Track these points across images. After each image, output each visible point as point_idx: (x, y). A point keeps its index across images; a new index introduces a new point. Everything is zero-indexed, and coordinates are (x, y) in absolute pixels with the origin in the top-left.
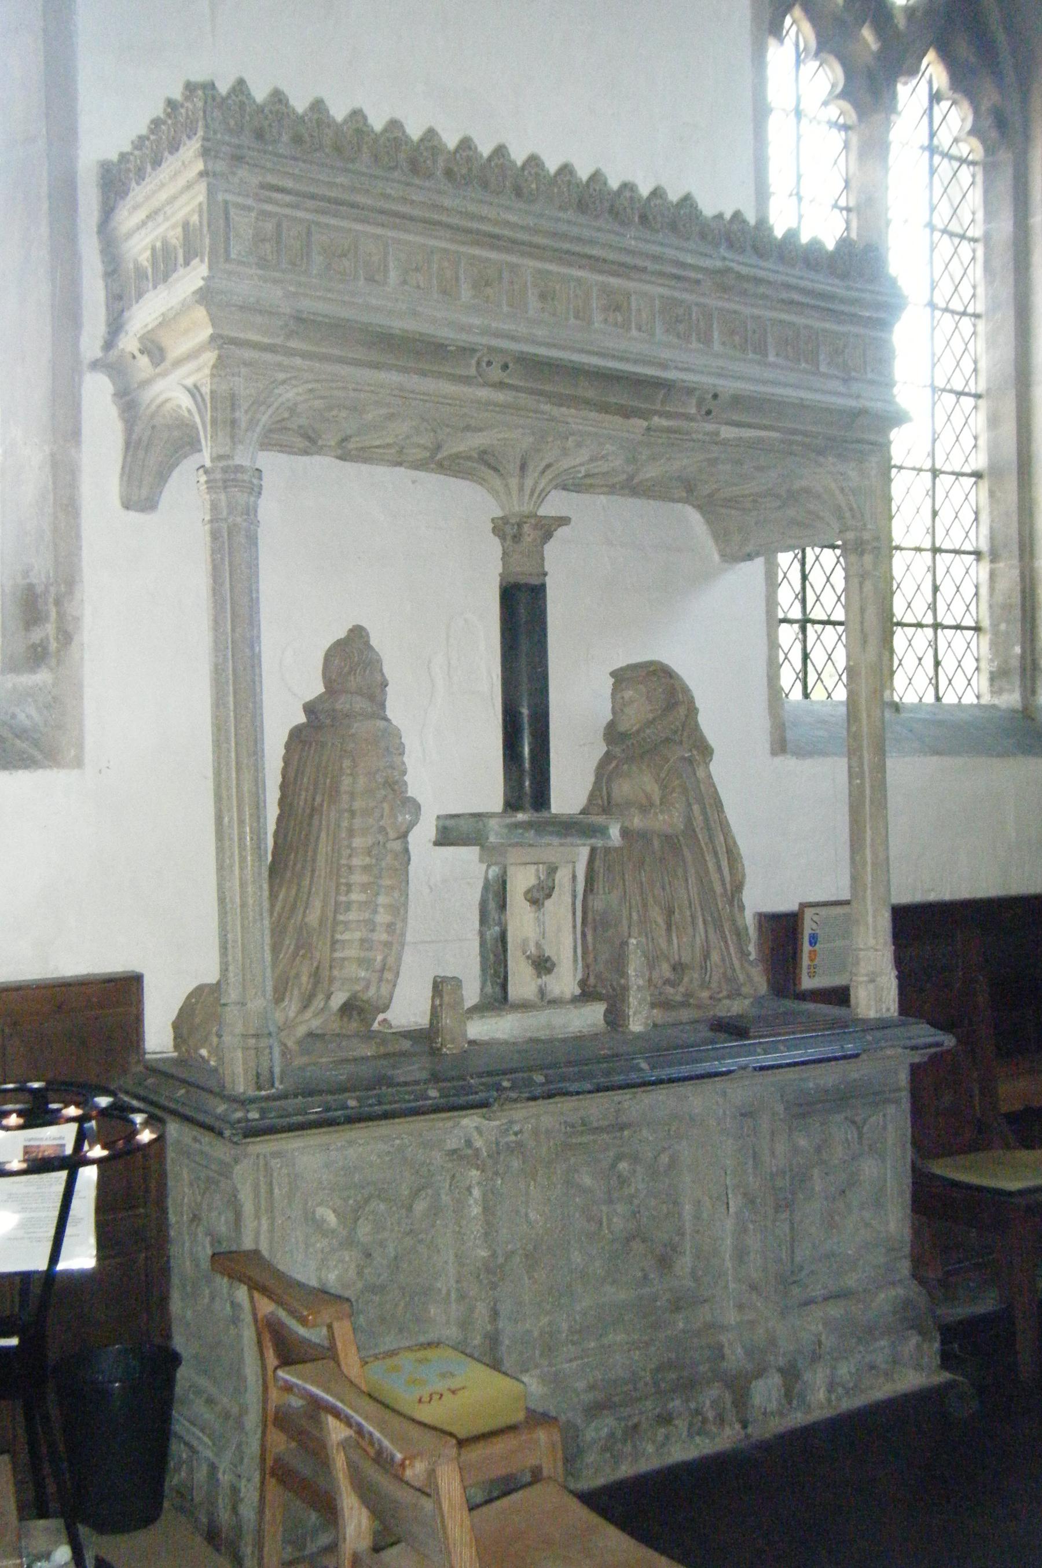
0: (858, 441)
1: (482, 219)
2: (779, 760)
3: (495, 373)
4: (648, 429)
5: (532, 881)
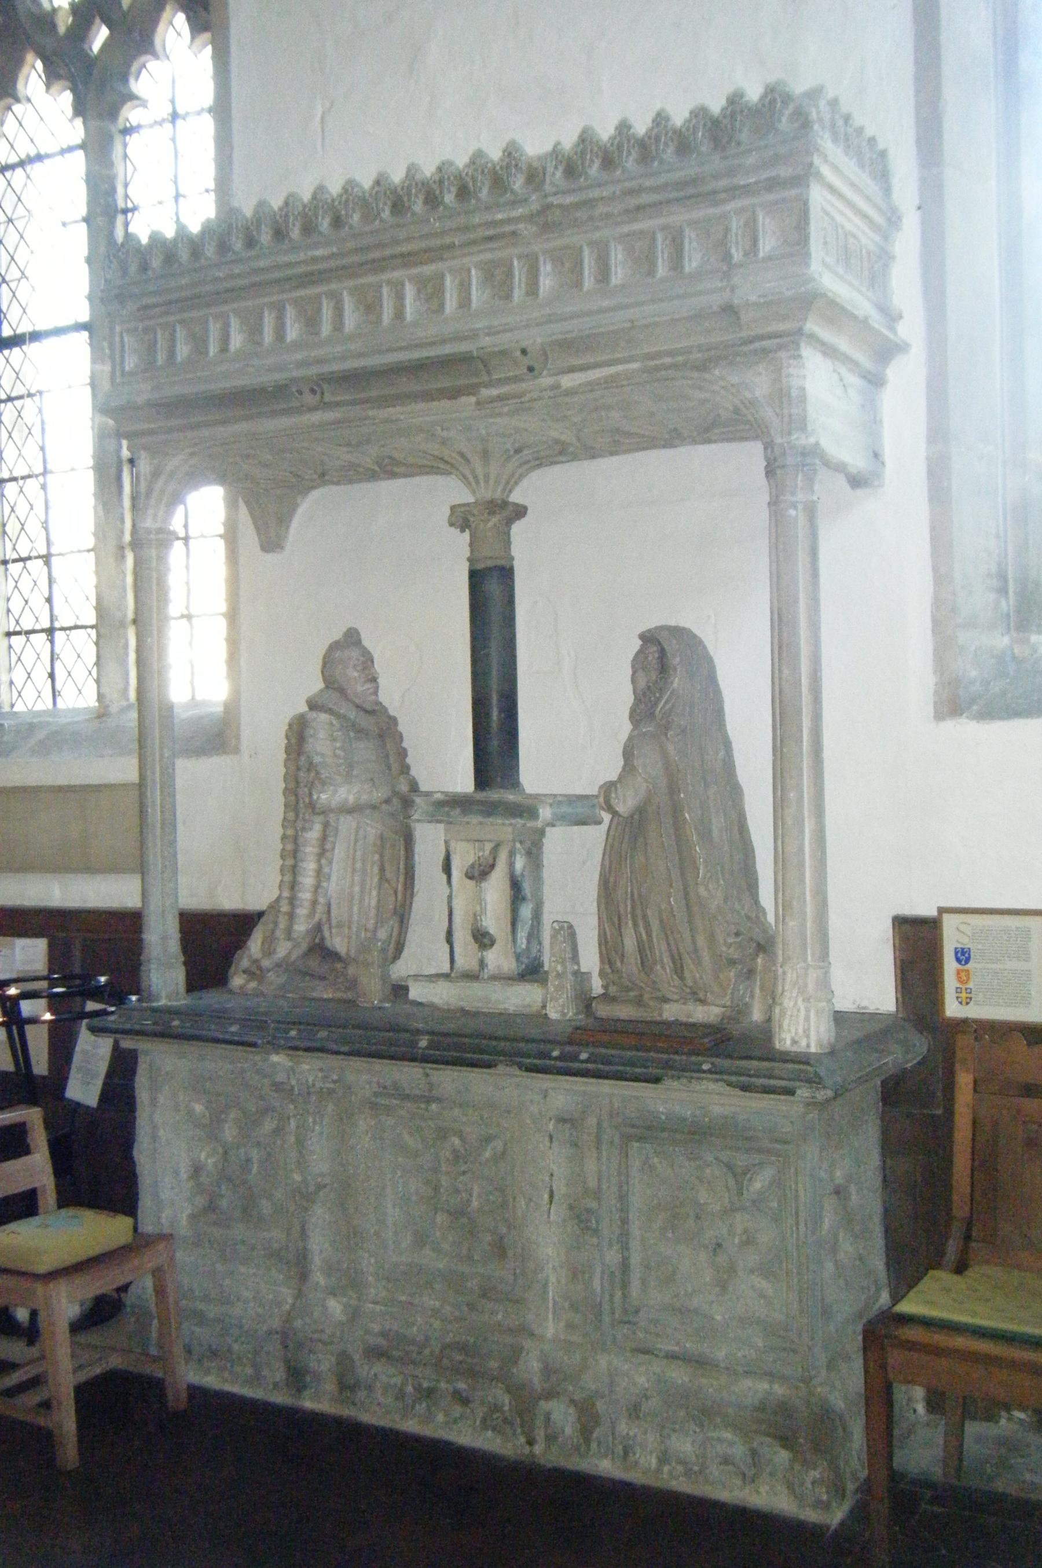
0: (751, 341)
1: (289, 265)
2: (950, 725)
3: (309, 399)
4: (478, 403)
5: (471, 859)
